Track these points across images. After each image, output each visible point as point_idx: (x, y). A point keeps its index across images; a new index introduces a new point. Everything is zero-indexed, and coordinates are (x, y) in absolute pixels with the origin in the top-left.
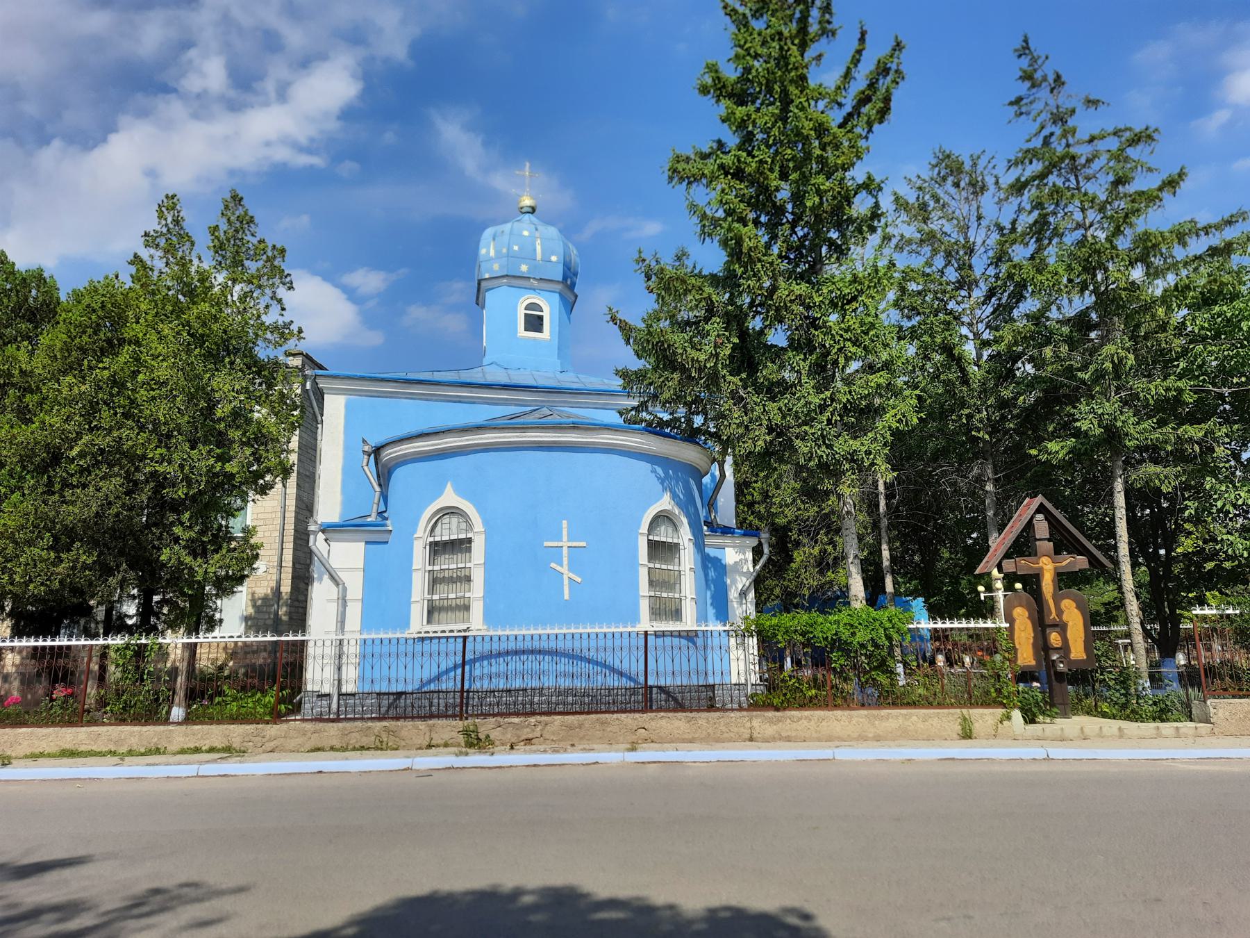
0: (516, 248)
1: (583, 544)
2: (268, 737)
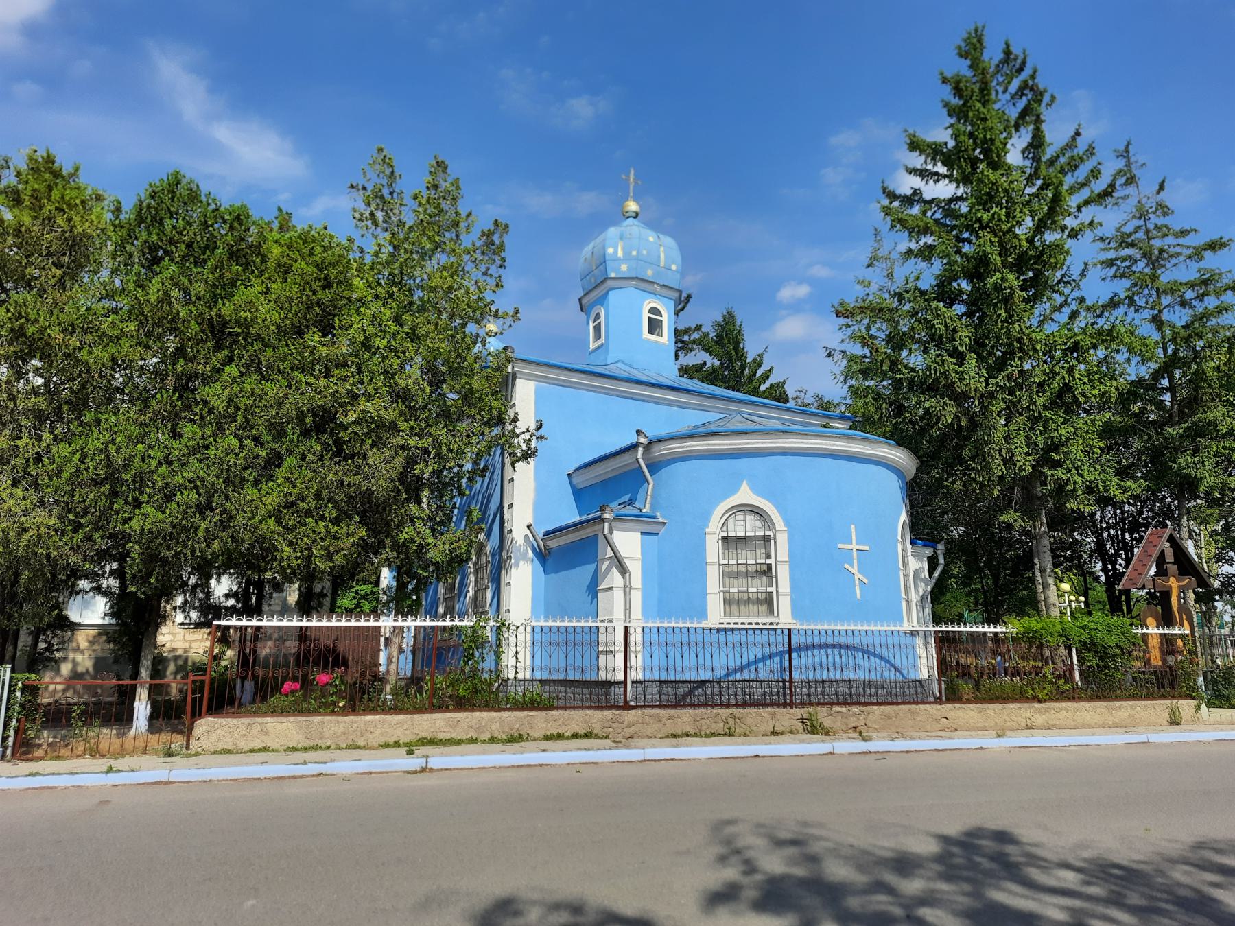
0: (645, 252)
1: (867, 548)
2: (626, 723)
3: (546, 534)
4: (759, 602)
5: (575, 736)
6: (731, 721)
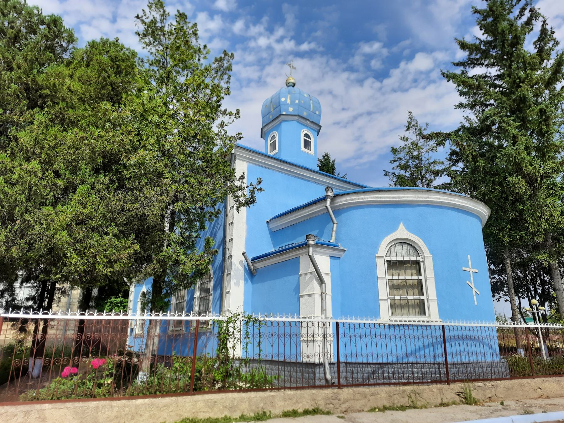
0: (302, 102)
3: (254, 259)
4: (413, 306)
5: (306, 412)
6: (413, 396)
